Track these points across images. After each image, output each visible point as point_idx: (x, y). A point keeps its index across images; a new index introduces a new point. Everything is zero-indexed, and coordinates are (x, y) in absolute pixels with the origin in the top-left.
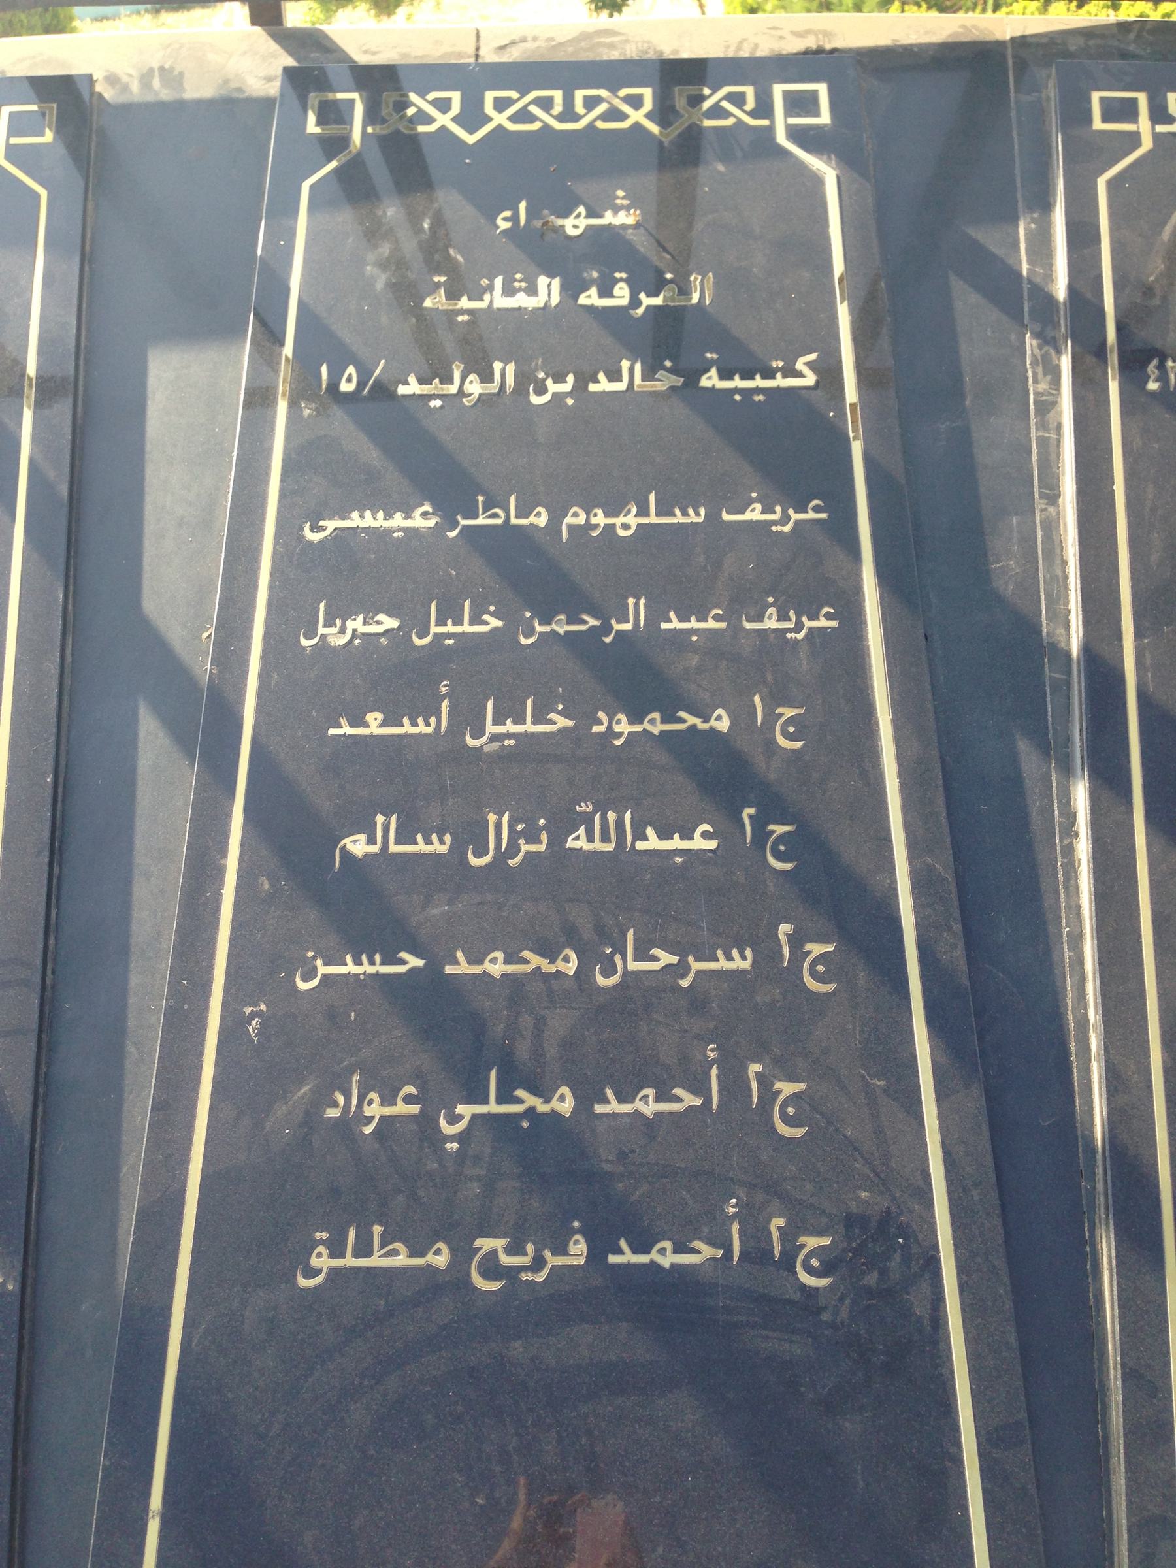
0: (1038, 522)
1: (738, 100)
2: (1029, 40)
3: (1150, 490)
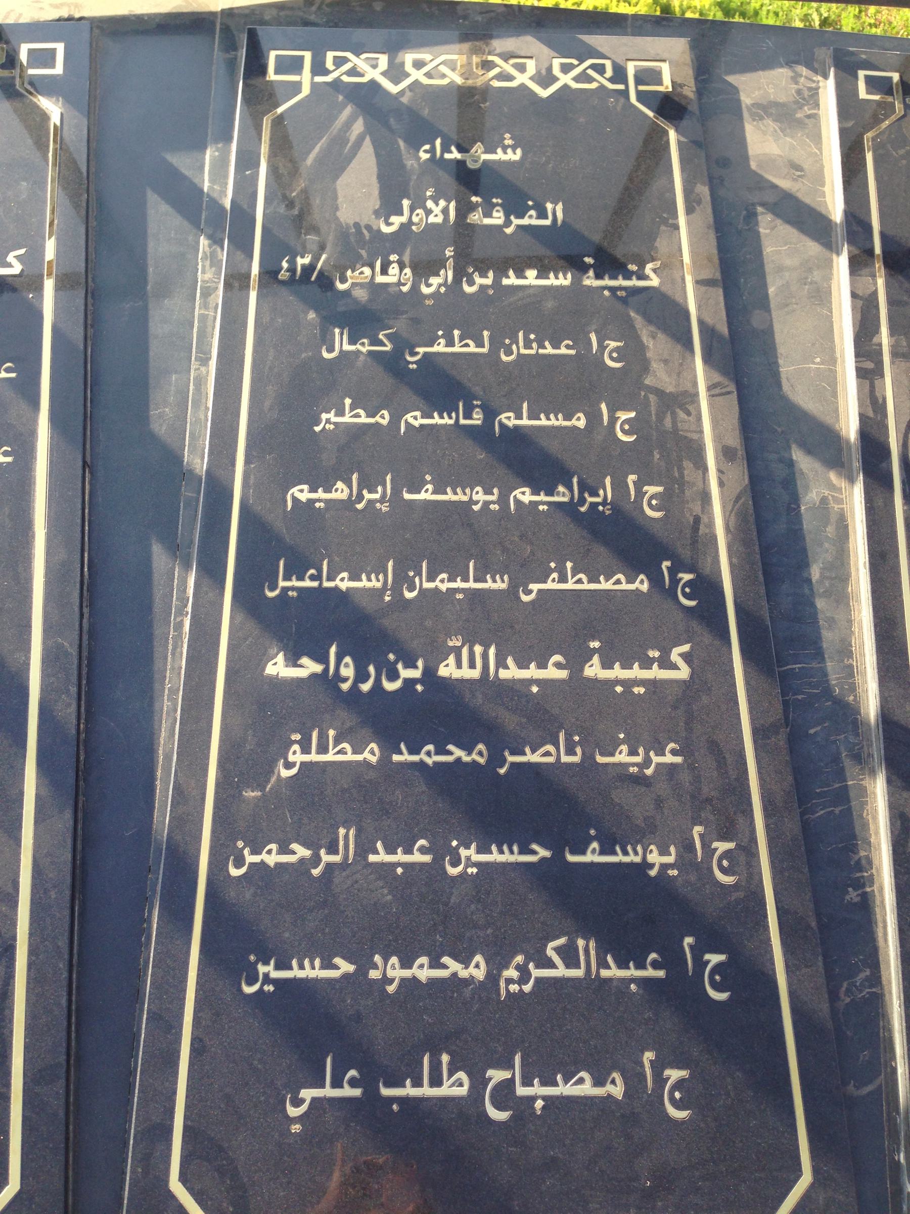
0: (192, 378)
2: (236, 11)
3: (272, 353)
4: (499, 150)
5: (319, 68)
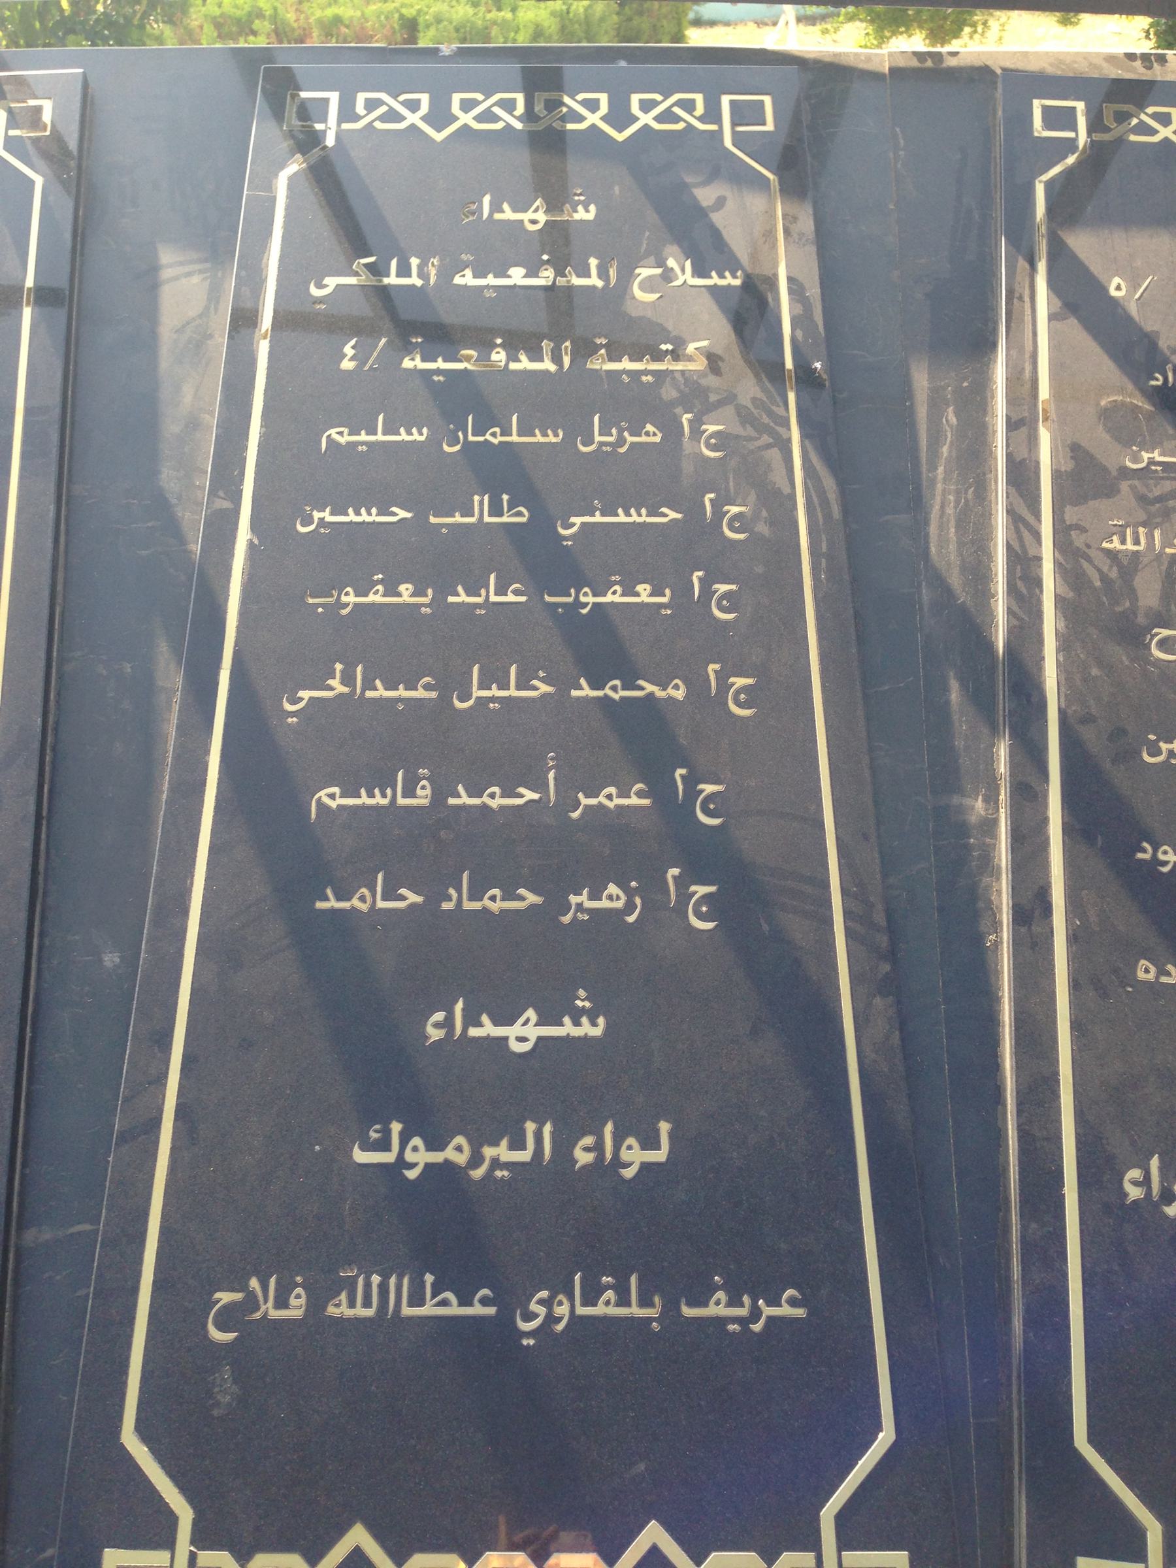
1: (689, 106)
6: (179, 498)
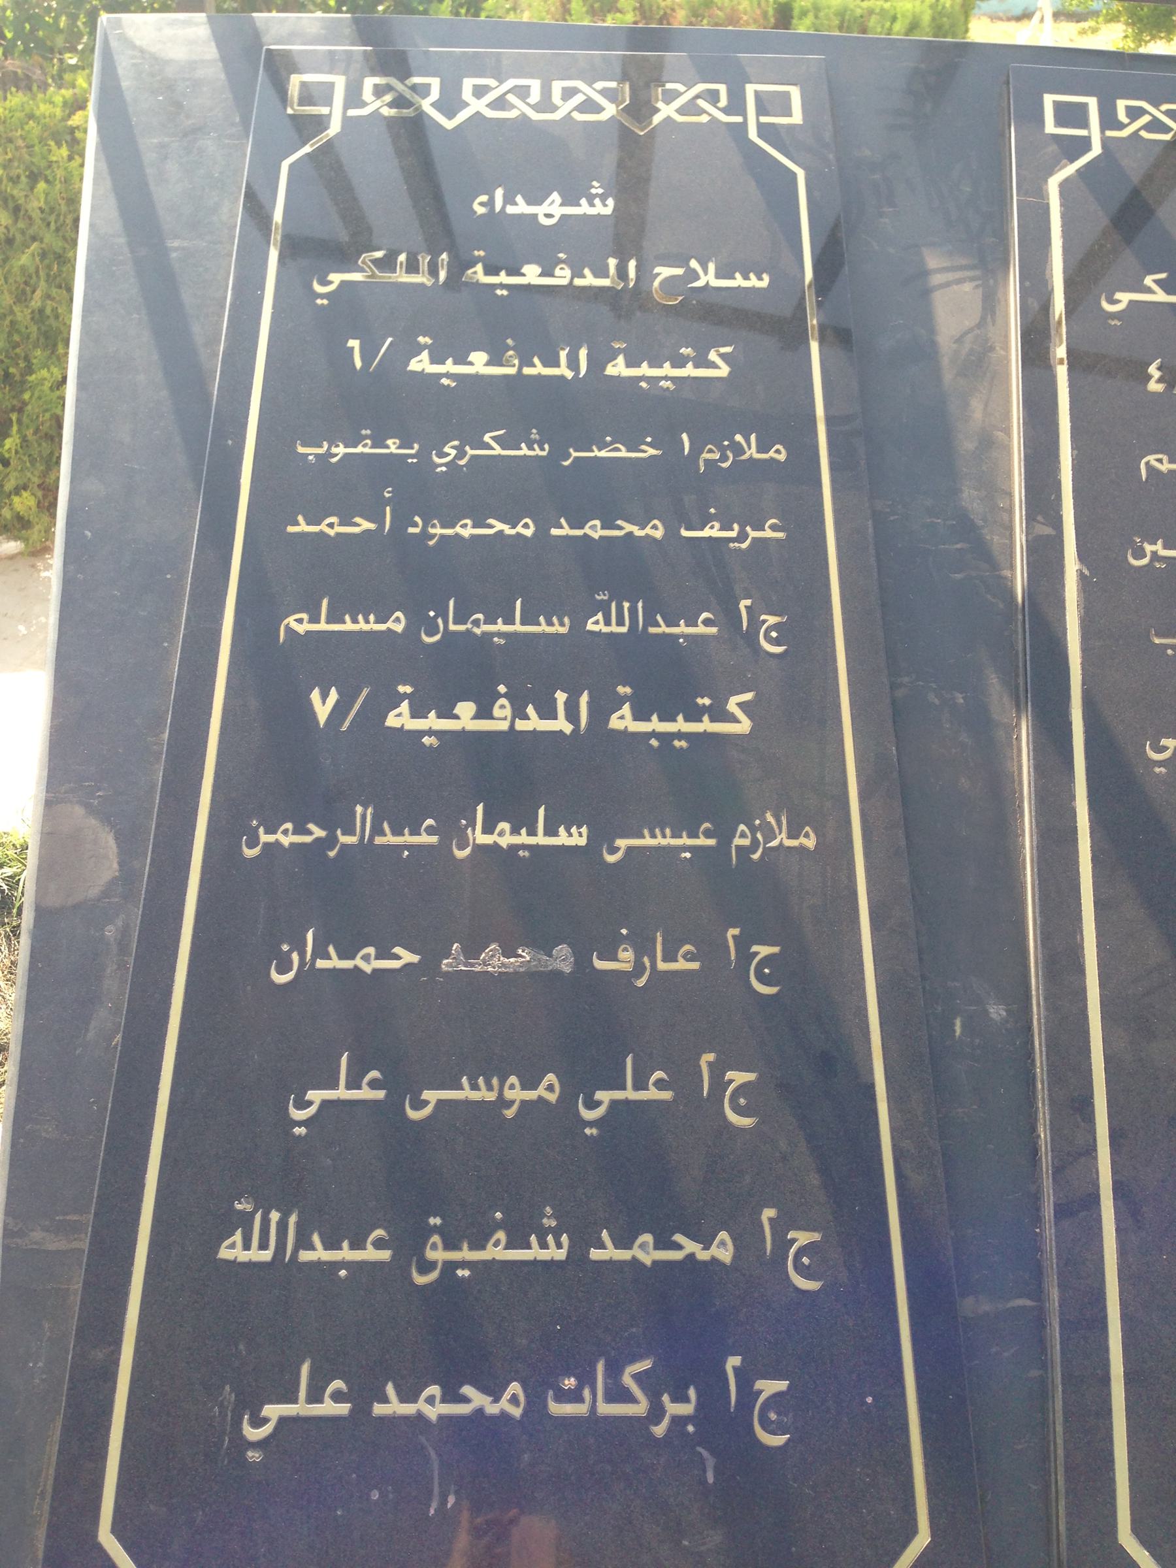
1: (522, 92)
4: (583, 201)
5: (1109, 120)
6: (985, 520)
